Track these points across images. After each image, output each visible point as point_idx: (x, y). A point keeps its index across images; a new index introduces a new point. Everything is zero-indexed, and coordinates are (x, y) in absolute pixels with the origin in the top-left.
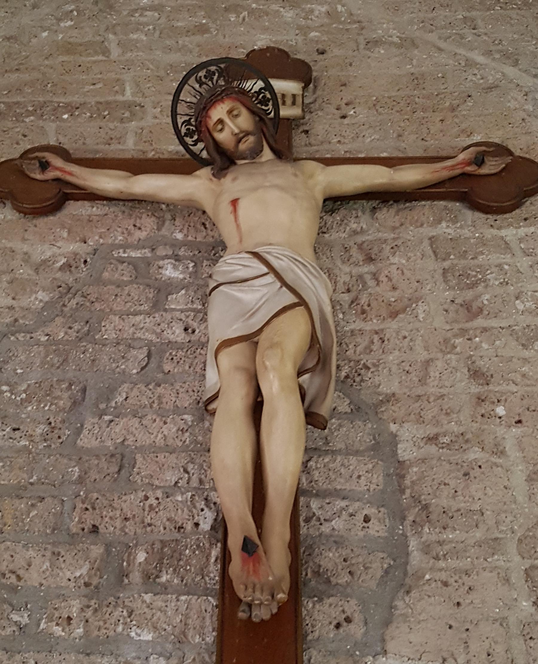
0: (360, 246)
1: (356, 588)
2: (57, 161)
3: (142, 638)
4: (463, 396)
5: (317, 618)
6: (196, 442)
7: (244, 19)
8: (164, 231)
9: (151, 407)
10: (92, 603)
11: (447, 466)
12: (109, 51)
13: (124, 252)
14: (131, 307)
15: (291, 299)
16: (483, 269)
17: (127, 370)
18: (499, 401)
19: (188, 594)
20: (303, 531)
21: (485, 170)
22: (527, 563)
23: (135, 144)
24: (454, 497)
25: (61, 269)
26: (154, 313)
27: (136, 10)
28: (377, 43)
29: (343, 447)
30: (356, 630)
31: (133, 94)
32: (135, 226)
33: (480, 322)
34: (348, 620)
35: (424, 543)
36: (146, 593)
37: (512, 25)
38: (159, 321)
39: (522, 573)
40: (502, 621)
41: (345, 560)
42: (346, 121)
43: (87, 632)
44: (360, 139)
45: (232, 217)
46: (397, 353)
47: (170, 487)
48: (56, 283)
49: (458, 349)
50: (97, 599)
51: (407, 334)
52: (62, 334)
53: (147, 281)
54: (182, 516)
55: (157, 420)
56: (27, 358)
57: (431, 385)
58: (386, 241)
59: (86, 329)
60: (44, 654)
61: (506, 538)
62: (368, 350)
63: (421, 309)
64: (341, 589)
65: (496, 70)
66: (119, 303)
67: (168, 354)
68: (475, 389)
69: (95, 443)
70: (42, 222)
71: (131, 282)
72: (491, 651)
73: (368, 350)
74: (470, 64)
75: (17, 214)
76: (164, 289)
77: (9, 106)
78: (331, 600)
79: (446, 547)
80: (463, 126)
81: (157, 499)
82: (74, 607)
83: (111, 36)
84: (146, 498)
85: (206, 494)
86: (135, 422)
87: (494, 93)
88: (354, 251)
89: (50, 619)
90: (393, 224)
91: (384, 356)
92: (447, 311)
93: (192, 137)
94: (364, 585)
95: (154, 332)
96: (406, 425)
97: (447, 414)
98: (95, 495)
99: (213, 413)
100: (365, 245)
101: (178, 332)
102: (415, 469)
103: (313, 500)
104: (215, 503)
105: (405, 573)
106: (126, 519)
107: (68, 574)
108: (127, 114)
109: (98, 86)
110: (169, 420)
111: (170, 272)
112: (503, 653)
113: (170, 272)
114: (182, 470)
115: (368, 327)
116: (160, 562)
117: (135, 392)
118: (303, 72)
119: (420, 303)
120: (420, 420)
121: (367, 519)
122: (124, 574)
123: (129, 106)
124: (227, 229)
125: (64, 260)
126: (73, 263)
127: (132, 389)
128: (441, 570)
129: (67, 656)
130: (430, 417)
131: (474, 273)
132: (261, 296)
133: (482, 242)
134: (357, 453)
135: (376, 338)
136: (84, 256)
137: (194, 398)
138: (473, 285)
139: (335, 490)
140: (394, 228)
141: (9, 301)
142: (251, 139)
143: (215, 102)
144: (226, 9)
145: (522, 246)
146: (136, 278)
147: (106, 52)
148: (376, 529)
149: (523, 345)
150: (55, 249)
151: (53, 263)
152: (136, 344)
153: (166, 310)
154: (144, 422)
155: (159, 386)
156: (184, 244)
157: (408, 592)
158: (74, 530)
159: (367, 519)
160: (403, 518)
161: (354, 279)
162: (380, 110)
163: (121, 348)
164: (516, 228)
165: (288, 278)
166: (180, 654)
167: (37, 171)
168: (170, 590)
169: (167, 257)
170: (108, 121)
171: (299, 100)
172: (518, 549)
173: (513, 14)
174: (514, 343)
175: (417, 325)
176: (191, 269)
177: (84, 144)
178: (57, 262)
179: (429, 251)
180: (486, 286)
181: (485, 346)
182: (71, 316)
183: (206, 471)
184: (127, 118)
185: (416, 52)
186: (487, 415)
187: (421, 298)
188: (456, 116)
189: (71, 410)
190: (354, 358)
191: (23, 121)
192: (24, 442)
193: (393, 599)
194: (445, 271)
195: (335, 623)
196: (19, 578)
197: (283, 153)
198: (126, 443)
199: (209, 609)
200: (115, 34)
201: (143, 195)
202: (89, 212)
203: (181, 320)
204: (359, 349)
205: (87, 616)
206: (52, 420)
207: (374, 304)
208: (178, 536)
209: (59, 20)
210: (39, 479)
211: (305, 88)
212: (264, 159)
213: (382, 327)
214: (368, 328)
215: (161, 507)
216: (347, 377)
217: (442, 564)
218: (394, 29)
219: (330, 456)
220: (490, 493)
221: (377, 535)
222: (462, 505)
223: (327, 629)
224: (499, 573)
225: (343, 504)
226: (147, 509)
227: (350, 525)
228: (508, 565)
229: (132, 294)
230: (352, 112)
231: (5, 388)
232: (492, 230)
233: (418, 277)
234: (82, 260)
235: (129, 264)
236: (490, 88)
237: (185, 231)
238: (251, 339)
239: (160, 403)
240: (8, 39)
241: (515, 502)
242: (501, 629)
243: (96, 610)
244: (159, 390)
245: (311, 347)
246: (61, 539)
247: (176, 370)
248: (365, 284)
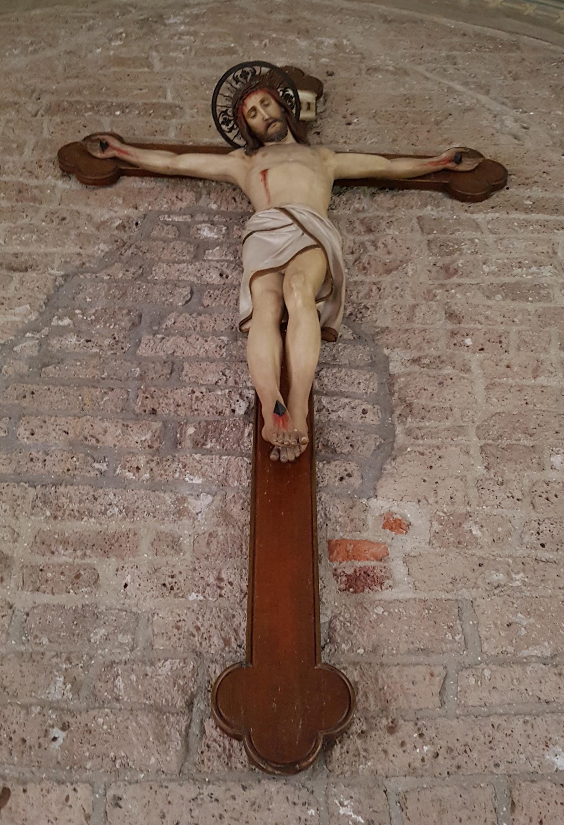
0: (362, 221)
1: (355, 455)
2: (115, 143)
3: (194, 482)
4: (441, 331)
5: (326, 473)
6: (231, 356)
7: (265, 45)
8: (202, 203)
9: (195, 329)
10: (155, 458)
11: (427, 378)
12: (153, 66)
13: (169, 217)
14: (176, 257)
15: (311, 242)
16: (458, 242)
17: (174, 303)
18: (467, 335)
19: (228, 455)
20: (316, 417)
21: (461, 168)
22: (483, 442)
23: (176, 136)
24: (431, 398)
25: (117, 228)
26: (195, 262)
27: (175, 35)
28: (376, 69)
29: (347, 362)
30: (356, 481)
31: (174, 98)
32: (177, 197)
33: (455, 280)
34: (349, 475)
35: (407, 429)
36: (196, 454)
38: (199, 268)
39: (478, 448)
40: (463, 478)
41: (347, 438)
42: (351, 127)
43: (152, 478)
44: (362, 141)
45: (262, 184)
46: (390, 298)
47: (211, 385)
48: (114, 238)
49: (438, 298)
50: (159, 456)
51: (398, 285)
52: (121, 275)
53: (188, 239)
54: (222, 405)
55: (200, 339)
56: (94, 291)
57: (417, 321)
58: (382, 218)
59: (140, 272)
60: (120, 490)
61: (468, 426)
62: (368, 296)
63: (410, 269)
64: (344, 456)
65: (470, 97)
66: (165, 254)
67: (207, 292)
68: (450, 326)
69: (150, 353)
70: (102, 192)
71: (175, 239)
72: (453, 496)
73: (368, 296)
74: (451, 90)
75: (80, 186)
78: (336, 462)
79: (424, 431)
80: (445, 136)
81: (202, 393)
82: (142, 461)
83: (154, 54)
84: (193, 392)
85: (240, 391)
86: (183, 340)
87: (471, 113)
88: (357, 224)
89: (124, 467)
90: (389, 206)
91: (380, 301)
92: (430, 271)
93: (227, 125)
94: (361, 453)
95: (196, 276)
96: (396, 350)
97: (428, 342)
98: (153, 389)
99: (247, 332)
100: (366, 220)
101: (214, 276)
102: (402, 379)
103: (323, 397)
104: (247, 398)
105: (393, 449)
106: (178, 406)
107: (136, 439)
108: (169, 113)
109: (144, 91)
110: (209, 340)
111: (206, 233)
112: (462, 497)
113: (206, 233)
114: (221, 374)
115: (368, 279)
116: (206, 434)
117: (181, 318)
118: (316, 86)
119: (409, 264)
120: (407, 346)
121: (364, 412)
122: (177, 443)
123: (170, 107)
124: (257, 194)
125: (118, 222)
126: (126, 224)
127: (178, 316)
128: (419, 445)
129: (138, 491)
130: (415, 344)
131: (452, 244)
132: (287, 239)
133: (458, 222)
134: (357, 367)
135: (374, 288)
136: (135, 219)
137: (229, 324)
138: (450, 253)
139: (341, 392)
140: (389, 209)
141: (78, 250)
142: (278, 125)
143: (250, 93)
144: (251, 38)
145: (489, 226)
147: (150, 66)
148: (370, 418)
149: (488, 297)
150: (112, 213)
151: (111, 224)
152: (181, 284)
153: (204, 260)
154: (189, 340)
155: (201, 315)
156: (217, 213)
157: (394, 459)
158: (138, 411)
159: (364, 412)
160: (393, 412)
161: (357, 245)
162: (378, 120)
163: (169, 286)
164: (485, 213)
165: (309, 228)
166: (223, 493)
167: (98, 151)
168: (213, 452)
169: (204, 222)
170: (153, 117)
171: (313, 107)
172: (476, 433)
173: (486, 56)
174: (481, 295)
175: (407, 279)
176: (224, 231)
177: (134, 134)
178: (114, 223)
179: (417, 227)
180: (461, 254)
181: (458, 296)
182: (127, 263)
183: (239, 375)
184: (169, 116)
185: (407, 79)
186: (458, 344)
188: (440, 129)
189: (130, 329)
190: (356, 301)
191: (83, 115)
192: (96, 350)
193: (383, 464)
195: (339, 477)
196: (97, 441)
197: (300, 139)
198: (175, 354)
199: (245, 465)
200: (158, 51)
201: (186, 171)
202: (139, 186)
203: (217, 268)
204: (360, 295)
205: (152, 466)
206: (116, 335)
207: (372, 263)
208: (219, 418)
209: (111, 40)
210: (109, 375)
211: (317, 99)
212: (287, 142)
213: (378, 280)
214: (368, 280)
215: (205, 399)
216: (351, 314)
217: (420, 442)
218: (390, 60)
219: (337, 369)
220: (458, 396)
221: (372, 422)
222: (437, 404)
223: (333, 480)
224: (461, 448)
225: (347, 400)
226: (194, 399)
227: (352, 412)
228: (469, 443)
229: (177, 248)
230: (355, 121)
231: (77, 311)
232: (466, 214)
233: (408, 245)
234: (135, 222)
235: (173, 226)
236: (467, 110)
237: (219, 203)
238: (279, 271)
239: (202, 327)
240: (69, 53)
241: (476, 403)
242: (461, 482)
243: (158, 463)
244: (201, 318)
245: (325, 281)
246: (127, 416)
247: (213, 304)
248: (365, 249)
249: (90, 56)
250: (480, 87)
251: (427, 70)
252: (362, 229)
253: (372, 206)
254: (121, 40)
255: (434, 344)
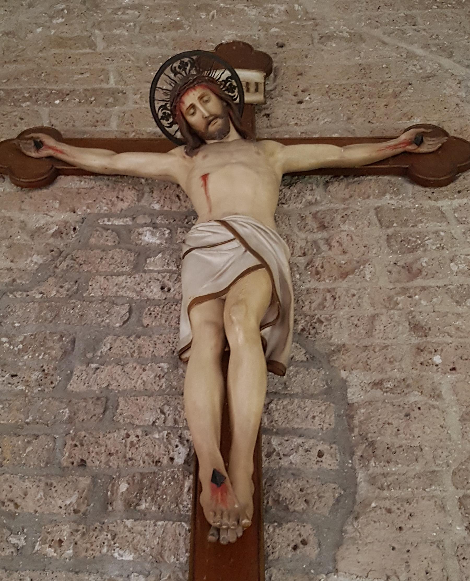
0: (315, 216)
1: (311, 514)
3: (124, 558)
4: (405, 347)
5: (277, 541)
7: (213, 17)
8: (143, 203)
9: (132, 356)
10: (81, 527)
11: (391, 408)
12: (95, 45)
13: (109, 221)
14: (114, 268)
16: (422, 236)
17: (111, 324)
18: (436, 351)
19: (164, 519)
20: (265, 464)
21: (423, 149)
22: (461, 493)
23: (118, 126)
24: (397, 435)
26: (135, 274)
27: (119, 9)
28: (329, 37)
29: (300, 391)
30: (311, 551)
31: (116, 83)
32: (118, 197)
33: (419, 282)
34: (304, 543)
35: (370, 475)
36: (128, 519)
37: (447, 22)
38: (139, 281)
39: (456, 501)
40: (439, 544)
41: (301, 490)
42: (302, 106)
43: (76, 553)
44: (315, 121)
46: (346, 309)
47: (148, 426)
48: (49, 248)
49: (400, 306)
50: (85, 524)
51: (355, 292)
52: (54, 293)
53: (129, 246)
54: (159, 452)
55: (138, 367)
56: (23, 314)
57: (377, 337)
58: (337, 210)
59: (75, 287)
60: (39, 572)
61: (442, 471)
62: (322, 306)
63: (368, 271)
64: (298, 515)
65: (434, 61)
66: (104, 265)
67: (147, 310)
68: (415, 340)
69: (83, 388)
70: (37, 194)
71: (114, 247)
72: (429, 569)
73: (322, 306)
74: (411, 56)
75: (15, 187)
76: (143, 253)
77: (8, 93)
78: (289, 525)
79: (390, 479)
80: (405, 110)
81: (137, 436)
82: (65, 531)
83: (97, 32)
84: (128, 436)
85: (180, 432)
86: (118, 369)
87: (432, 81)
88: (309, 220)
89: (44, 542)
90: (343, 196)
91: (335, 312)
92: (390, 272)
94: (318, 512)
95: (135, 290)
96: (354, 372)
97: (391, 362)
98: (83, 433)
99: (186, 362)
100: (319, 214)
101: (155, 290)
102: (363, 411)
103: (273, 437)
104: (188, 441)
105: (354, 502)
106: (110, 454)
107: (60, 503)
108: (111, 100)
109: (86, 75)
110: (147, 368)
111: (149, 238)
112: (439, 571)
113: (149, 238)
114: (159, 411)
115: (321, 286)
116: (140, 491)
117: (118, 343)
118: (264, 63)
119: (367, 265)
120: (367, 367)
121: (320, 454)
122: (108, 502)
123: (113, 92)
125: (56, 228)
126: (63, 230)
127: (115, 340)
128: (385, 499)
129: (58, 574)
130: (375, 365)
131: (414, 239)
132: (228, 259)
133: (422, 211)
134: (312, 396)
135: (328, 296)
136: (73, 224)
137: (170, 348)
138: (413, 250)
139: (293, 428)
140: (344, 200)
141: (8, 264)
144: (198, 8)
145: (456, 215)
146: (119, 243)
147: (92, 45)
148: (329, 463)
149: (457, 302)
150: (48, 218)
151: (47, 230)
152: (119, 301)
153: (145, 271)
154: (126, 369)
155: (139, 338)
156: (161, 213)
157: (356, 518)
158: (65, 464)
159: (320, 454)
160: (352, 454)
161: (309, 244)
162: (332, 96)
163: (106, 304)
164: (451, 199)
165: (252, 243)
166: (158, 572)
168: (148, 516)
169: (146, 225)
170: (94, 106)
171: (261, 87)
172: (452, 480)
173: (448, 12)
174: (449, 300)
175: (365, 284)
176: (167, 235)
177: (73, 126)
178: (50, 229)
179: (374, 219)
180: (425, 251)
181: (424, 303)
182: (62, 277)
183: (180, 412)
184: (111, 103)
185: (363, 45)
187: (368, 261)
188: (399, 102)
189: (62, 358)
190: (309, 313)
191: (20, 106)
192: (21, 387)
193: (343, 525)
194: (389, 237)
195: (292, 545)
196: (17, 506)
197: (247, 134)
198: (110, 388)
199: (183, 533)
200: (100, 29)
202: (78, 186)
203: (158, 280)
204: (313, 305)
205: (76, 539)
206: (45, 367)
207: (326, 266)
208: (155, 469)
209: (52, 17)
210: (34, 419)
211: (266, 77)
213: (333, 286)
214: (321, 287)
215: (141, 444)
216: (303, 330)
217: (386, 493)
218: (344, 26)
219: (288, 399)
220: (428, 431)
221: (329, 468)
222: (404, 442)
223: (286, 550)
224: (436, 502)
225: (300, 441)
226: (128, 445)
228: (444, 494)
229: (115, 257)
230: (307, 98)
232: (430, 201)
233: (365, 243)
234: (72, 228)
235: (113, 231)
236: (428, 77)
237: (162, 202)
238: (219, 297)
239: (140, 353)
240: (7, 34)
241: (450, 440)
242: (438, 551)
243: (84, 534)
244: (139, 341)
247: (153, 324)
248: (318, 248)
249: (30, 36)
250: (442, 49)
251: (384, 33)
252: (315, 225)
253: (325, 198)
254: (63, 17)
255: (398, 364)
